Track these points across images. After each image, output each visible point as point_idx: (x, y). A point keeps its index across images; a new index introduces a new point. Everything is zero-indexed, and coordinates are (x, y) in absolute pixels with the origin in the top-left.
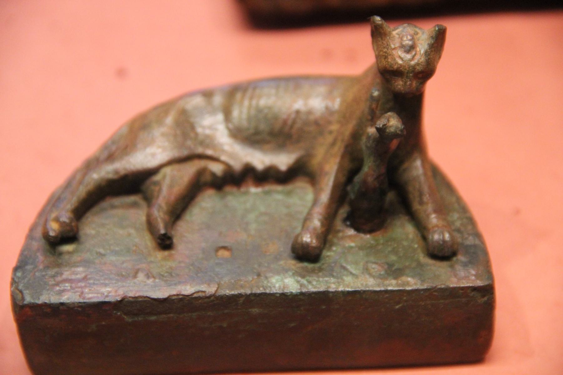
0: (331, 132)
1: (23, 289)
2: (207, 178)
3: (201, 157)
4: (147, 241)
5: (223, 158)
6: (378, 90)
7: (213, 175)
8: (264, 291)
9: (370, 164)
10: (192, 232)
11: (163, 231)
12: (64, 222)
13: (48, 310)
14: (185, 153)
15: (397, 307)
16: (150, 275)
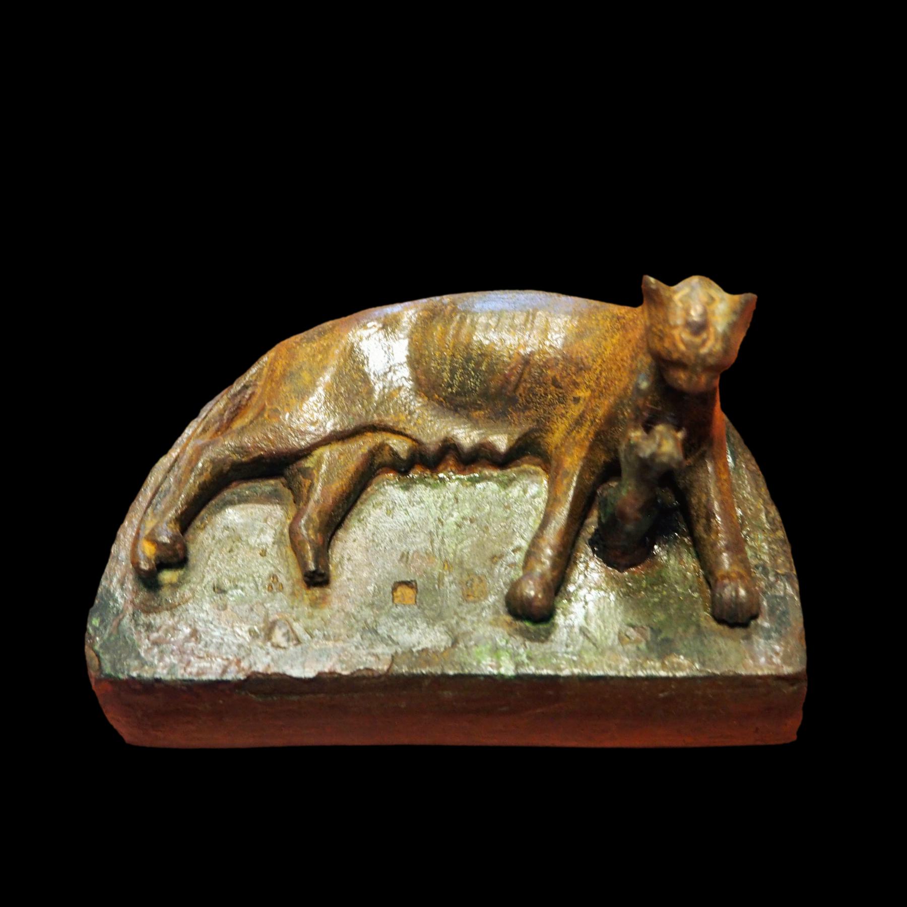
0: (577, 400)
1: (101, 651)
2: (386, 457)
3: (374, 428)
4: (289, 575)
5: (411, 430)
6: (648, 380)
7: (395, 454)
8: (461, 672)
9: (630, 488)
10: (358, 553)
11: (312, 567)
12: (165, 544)
13: (138, 687)
14: (350, 423)
15: (661, 695)
16: (292, 635)
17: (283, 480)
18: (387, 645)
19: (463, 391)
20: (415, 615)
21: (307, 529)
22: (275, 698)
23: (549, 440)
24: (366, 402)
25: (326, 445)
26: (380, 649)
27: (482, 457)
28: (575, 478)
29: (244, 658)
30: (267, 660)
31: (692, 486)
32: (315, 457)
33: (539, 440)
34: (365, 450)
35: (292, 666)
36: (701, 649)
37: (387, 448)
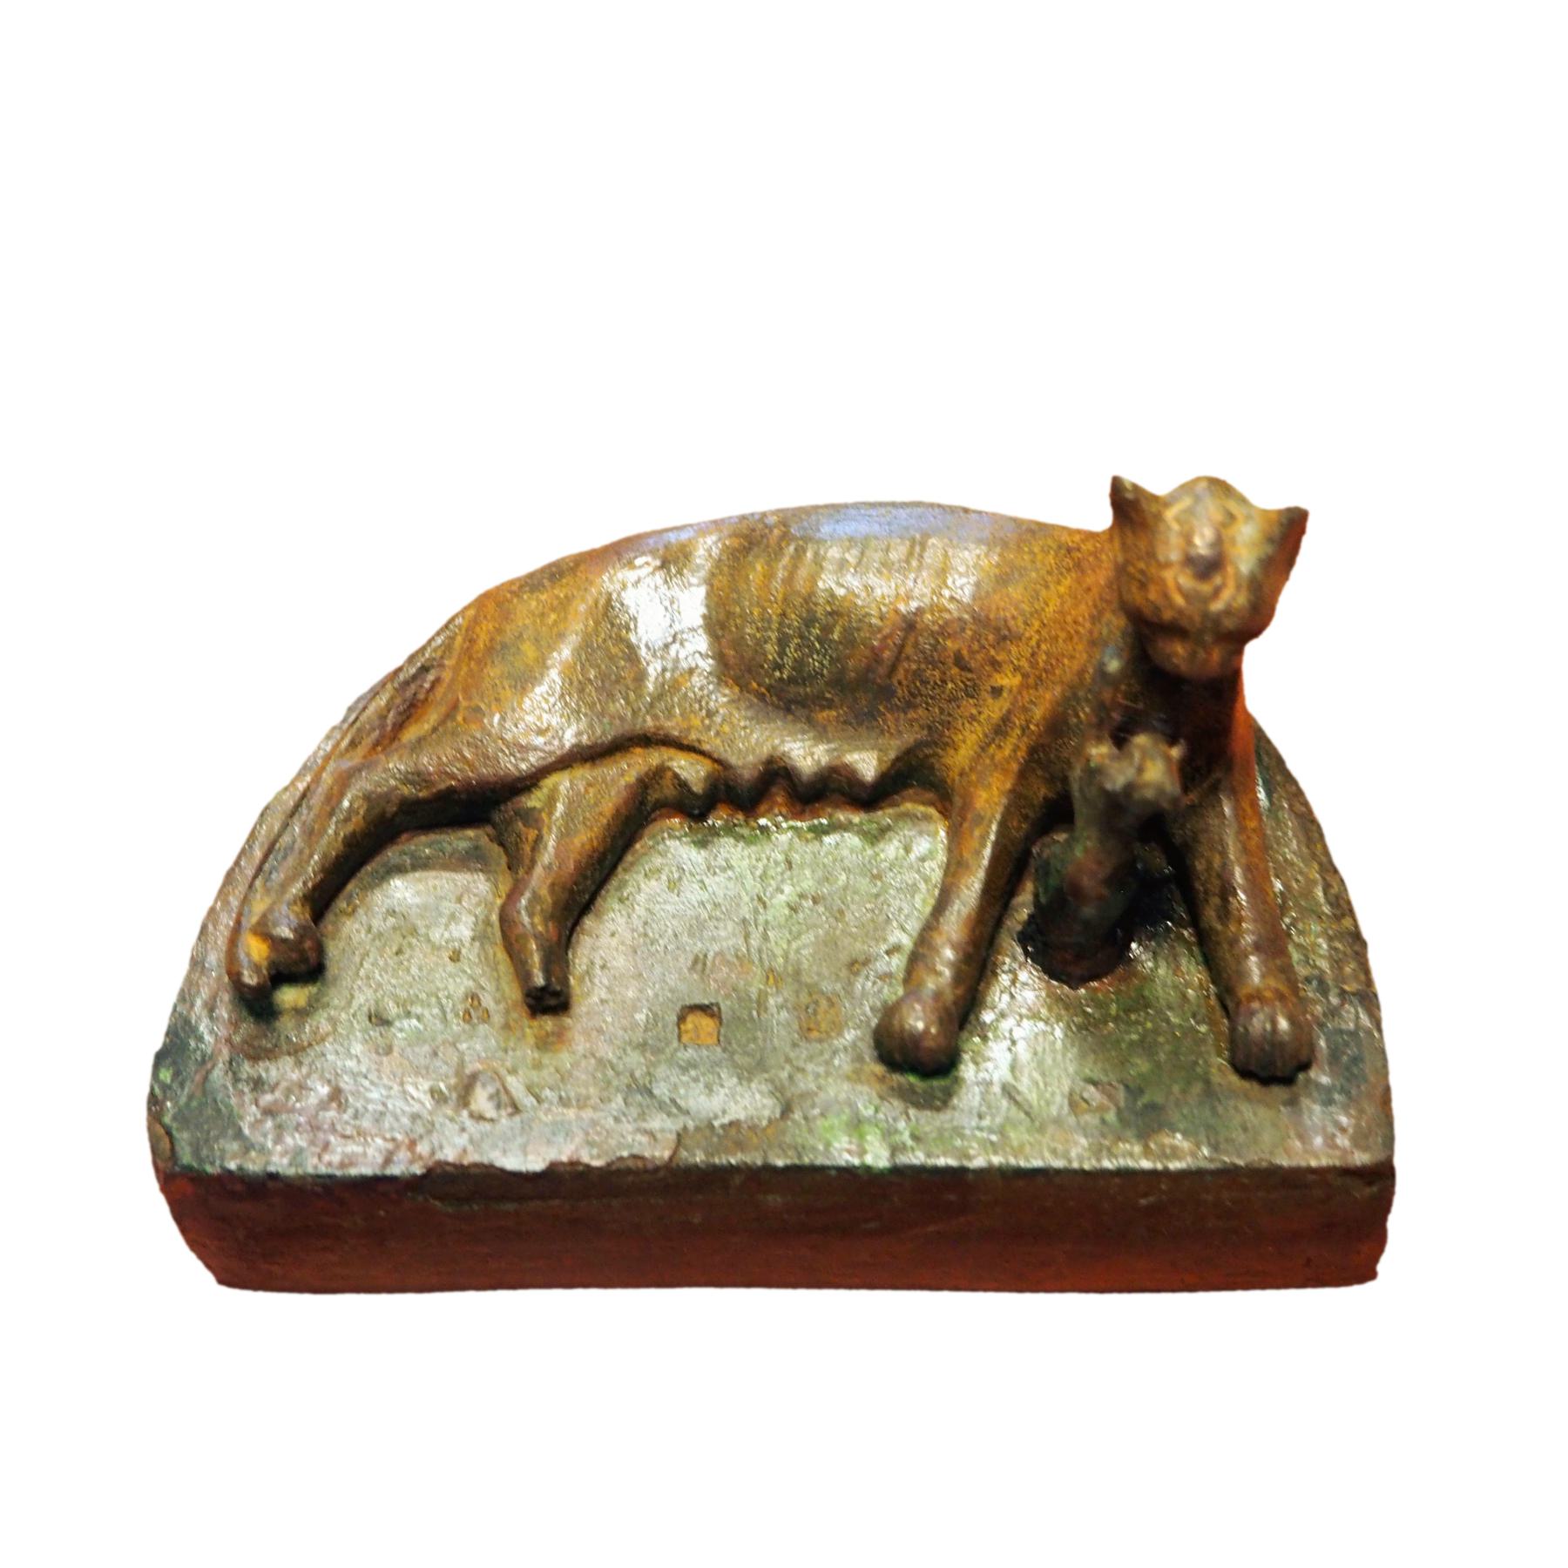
0: (997, 692)
1: (175, 1125)
2: (668, 790)
3: (647, 740)
4: (499, 993)
5: (711, 743)
6: (1119, 656)
7: (683, 785)
8: (797, 1161)
9: (1089, 844)
10: (618, 955)
11: (539, 980)
12: (285, 941)
13: (239, 1187)
14: (605, 732)
15: (1143, 1202)
16: (504, 1098)
17: (489, 829)
18: (669, 1114)
19: (801, 675)
20: (718, 1064)
21: (531, 915)
22: (476, 1207)
23: (948, 761)
24: (632, 695)
25: (563, 769)
26: (657, 1122)
27: (833, 791)
28: (994, 827)
29: (421, 1137)
30: (462, 1140)
31: (1196, 839)
32: (545, 790)
33: (933, 760)
34: (631, 777)
35: (505, 1152)
36: (1212, 1121)
37: (669, 774)
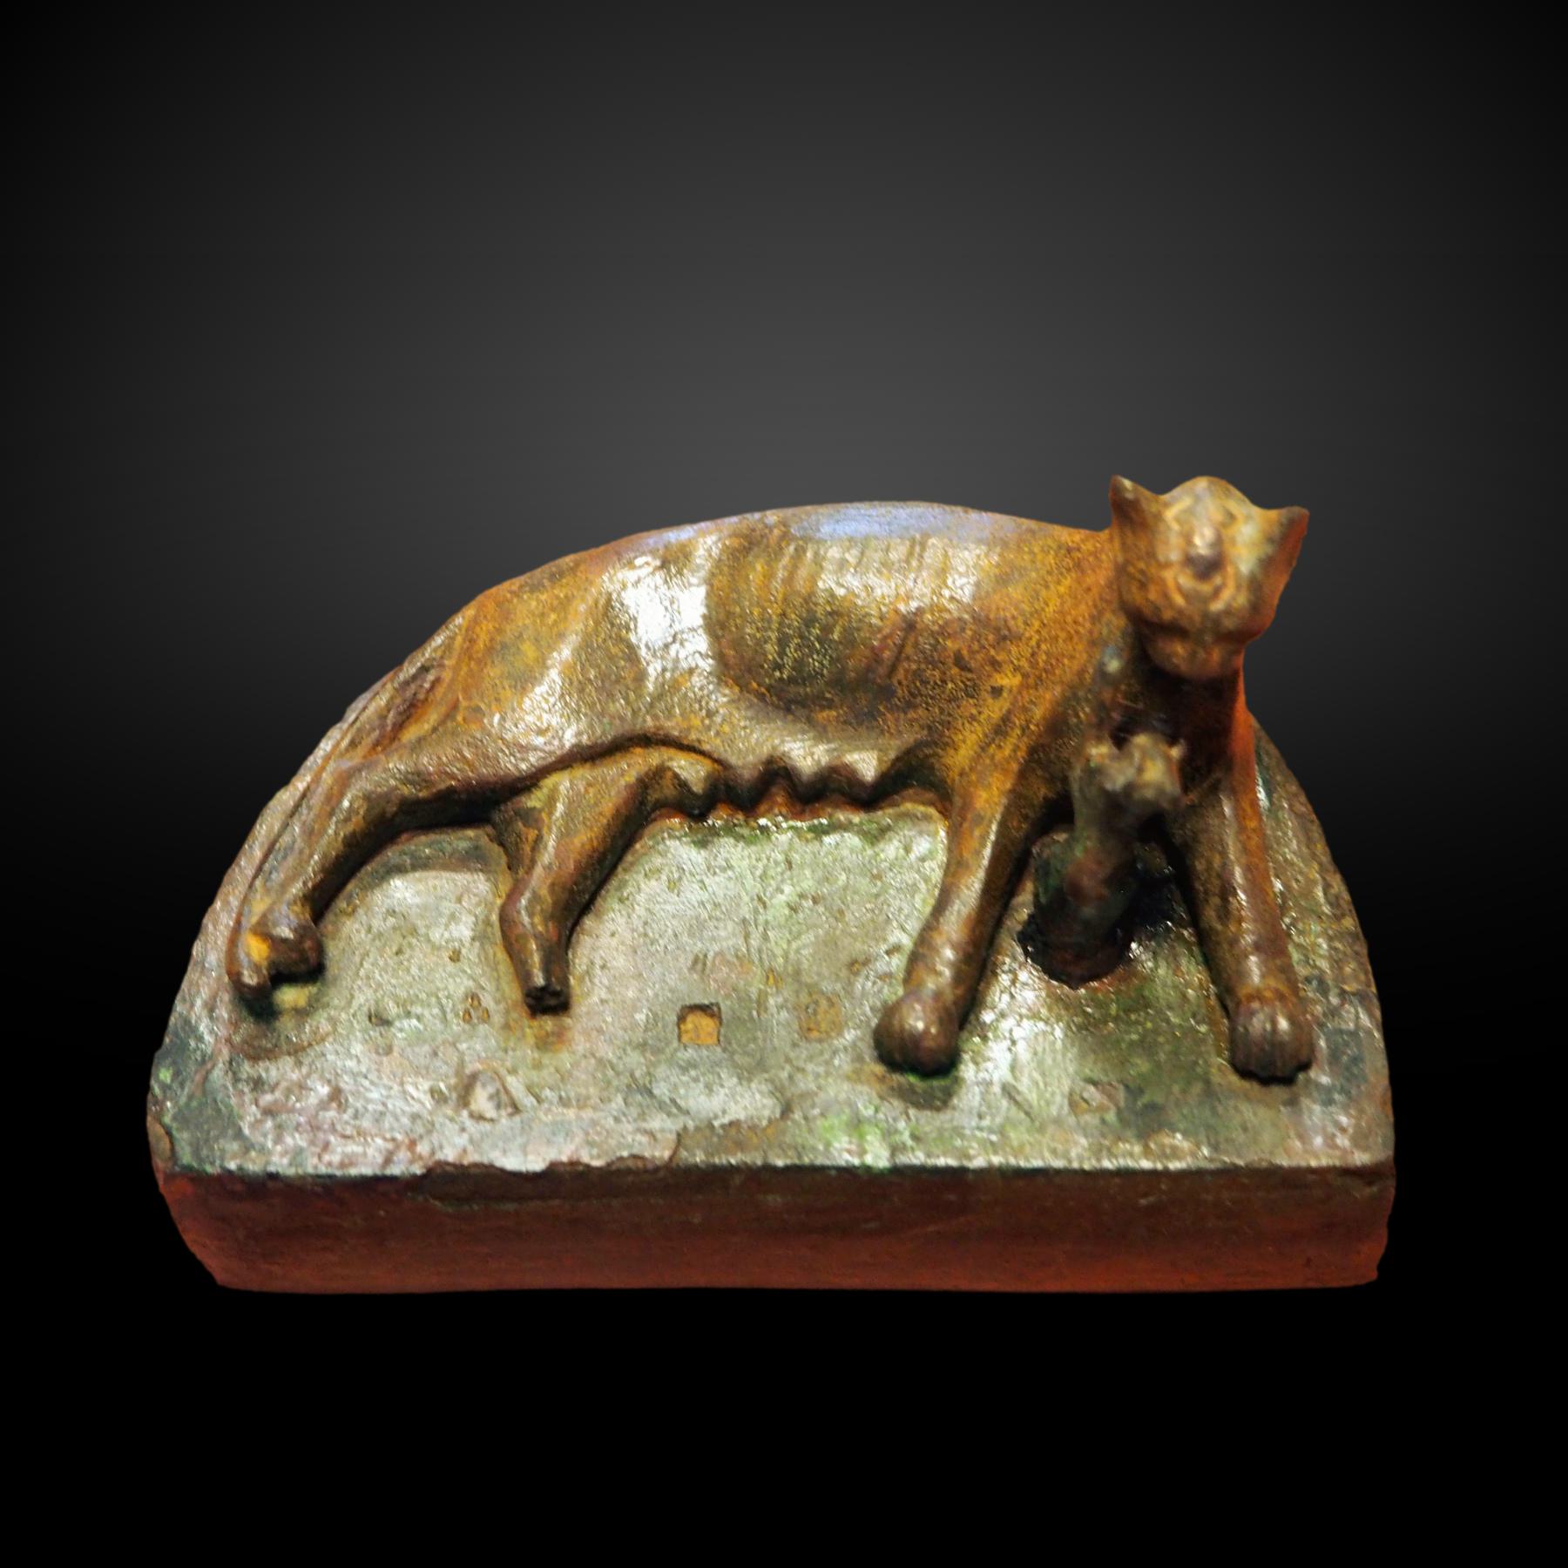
0: (997, 692)
1: (175, 1125)
2: (668, 790)
3: (647, 740)
4: (499, 993)
5: (711, 743)
6: (1119, 656)
7: (683, 785)
8: (797, 1161)
9: (1089, 844)
10: (618, 955)
11: (539, 980)
12: (285, 941)
13: (239, 1187)
14: (605, 732)
15: (1143, 1202)
16: (504, 1098)
17: (489, 829)
18: (669, 1114)
19: (801, 675)
20: (718, 1064)
21: (531, 915)
22: (476, 1207)
23: (948, 761)
24: (632, 695)
25: (563, 769)
26: (657, 1122)
27: (833, 791)
28: (994, 827)
29: (421, 1137)
30: (462, 1140)
31: (1196, 839)
32: (545, 790)
33: (933, 760)
34: (631, 777)
35: (505, 1152)
36: (1212, 1121)
37: (669, 774)
